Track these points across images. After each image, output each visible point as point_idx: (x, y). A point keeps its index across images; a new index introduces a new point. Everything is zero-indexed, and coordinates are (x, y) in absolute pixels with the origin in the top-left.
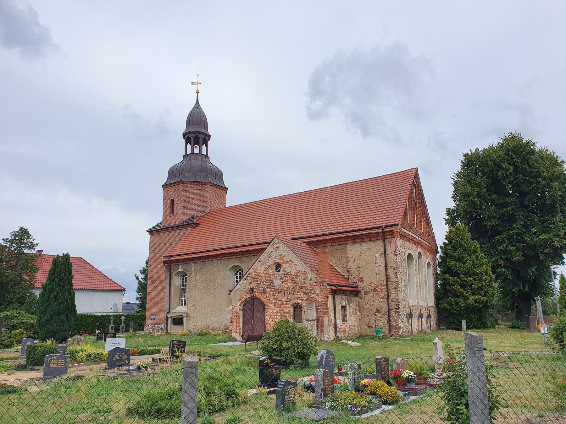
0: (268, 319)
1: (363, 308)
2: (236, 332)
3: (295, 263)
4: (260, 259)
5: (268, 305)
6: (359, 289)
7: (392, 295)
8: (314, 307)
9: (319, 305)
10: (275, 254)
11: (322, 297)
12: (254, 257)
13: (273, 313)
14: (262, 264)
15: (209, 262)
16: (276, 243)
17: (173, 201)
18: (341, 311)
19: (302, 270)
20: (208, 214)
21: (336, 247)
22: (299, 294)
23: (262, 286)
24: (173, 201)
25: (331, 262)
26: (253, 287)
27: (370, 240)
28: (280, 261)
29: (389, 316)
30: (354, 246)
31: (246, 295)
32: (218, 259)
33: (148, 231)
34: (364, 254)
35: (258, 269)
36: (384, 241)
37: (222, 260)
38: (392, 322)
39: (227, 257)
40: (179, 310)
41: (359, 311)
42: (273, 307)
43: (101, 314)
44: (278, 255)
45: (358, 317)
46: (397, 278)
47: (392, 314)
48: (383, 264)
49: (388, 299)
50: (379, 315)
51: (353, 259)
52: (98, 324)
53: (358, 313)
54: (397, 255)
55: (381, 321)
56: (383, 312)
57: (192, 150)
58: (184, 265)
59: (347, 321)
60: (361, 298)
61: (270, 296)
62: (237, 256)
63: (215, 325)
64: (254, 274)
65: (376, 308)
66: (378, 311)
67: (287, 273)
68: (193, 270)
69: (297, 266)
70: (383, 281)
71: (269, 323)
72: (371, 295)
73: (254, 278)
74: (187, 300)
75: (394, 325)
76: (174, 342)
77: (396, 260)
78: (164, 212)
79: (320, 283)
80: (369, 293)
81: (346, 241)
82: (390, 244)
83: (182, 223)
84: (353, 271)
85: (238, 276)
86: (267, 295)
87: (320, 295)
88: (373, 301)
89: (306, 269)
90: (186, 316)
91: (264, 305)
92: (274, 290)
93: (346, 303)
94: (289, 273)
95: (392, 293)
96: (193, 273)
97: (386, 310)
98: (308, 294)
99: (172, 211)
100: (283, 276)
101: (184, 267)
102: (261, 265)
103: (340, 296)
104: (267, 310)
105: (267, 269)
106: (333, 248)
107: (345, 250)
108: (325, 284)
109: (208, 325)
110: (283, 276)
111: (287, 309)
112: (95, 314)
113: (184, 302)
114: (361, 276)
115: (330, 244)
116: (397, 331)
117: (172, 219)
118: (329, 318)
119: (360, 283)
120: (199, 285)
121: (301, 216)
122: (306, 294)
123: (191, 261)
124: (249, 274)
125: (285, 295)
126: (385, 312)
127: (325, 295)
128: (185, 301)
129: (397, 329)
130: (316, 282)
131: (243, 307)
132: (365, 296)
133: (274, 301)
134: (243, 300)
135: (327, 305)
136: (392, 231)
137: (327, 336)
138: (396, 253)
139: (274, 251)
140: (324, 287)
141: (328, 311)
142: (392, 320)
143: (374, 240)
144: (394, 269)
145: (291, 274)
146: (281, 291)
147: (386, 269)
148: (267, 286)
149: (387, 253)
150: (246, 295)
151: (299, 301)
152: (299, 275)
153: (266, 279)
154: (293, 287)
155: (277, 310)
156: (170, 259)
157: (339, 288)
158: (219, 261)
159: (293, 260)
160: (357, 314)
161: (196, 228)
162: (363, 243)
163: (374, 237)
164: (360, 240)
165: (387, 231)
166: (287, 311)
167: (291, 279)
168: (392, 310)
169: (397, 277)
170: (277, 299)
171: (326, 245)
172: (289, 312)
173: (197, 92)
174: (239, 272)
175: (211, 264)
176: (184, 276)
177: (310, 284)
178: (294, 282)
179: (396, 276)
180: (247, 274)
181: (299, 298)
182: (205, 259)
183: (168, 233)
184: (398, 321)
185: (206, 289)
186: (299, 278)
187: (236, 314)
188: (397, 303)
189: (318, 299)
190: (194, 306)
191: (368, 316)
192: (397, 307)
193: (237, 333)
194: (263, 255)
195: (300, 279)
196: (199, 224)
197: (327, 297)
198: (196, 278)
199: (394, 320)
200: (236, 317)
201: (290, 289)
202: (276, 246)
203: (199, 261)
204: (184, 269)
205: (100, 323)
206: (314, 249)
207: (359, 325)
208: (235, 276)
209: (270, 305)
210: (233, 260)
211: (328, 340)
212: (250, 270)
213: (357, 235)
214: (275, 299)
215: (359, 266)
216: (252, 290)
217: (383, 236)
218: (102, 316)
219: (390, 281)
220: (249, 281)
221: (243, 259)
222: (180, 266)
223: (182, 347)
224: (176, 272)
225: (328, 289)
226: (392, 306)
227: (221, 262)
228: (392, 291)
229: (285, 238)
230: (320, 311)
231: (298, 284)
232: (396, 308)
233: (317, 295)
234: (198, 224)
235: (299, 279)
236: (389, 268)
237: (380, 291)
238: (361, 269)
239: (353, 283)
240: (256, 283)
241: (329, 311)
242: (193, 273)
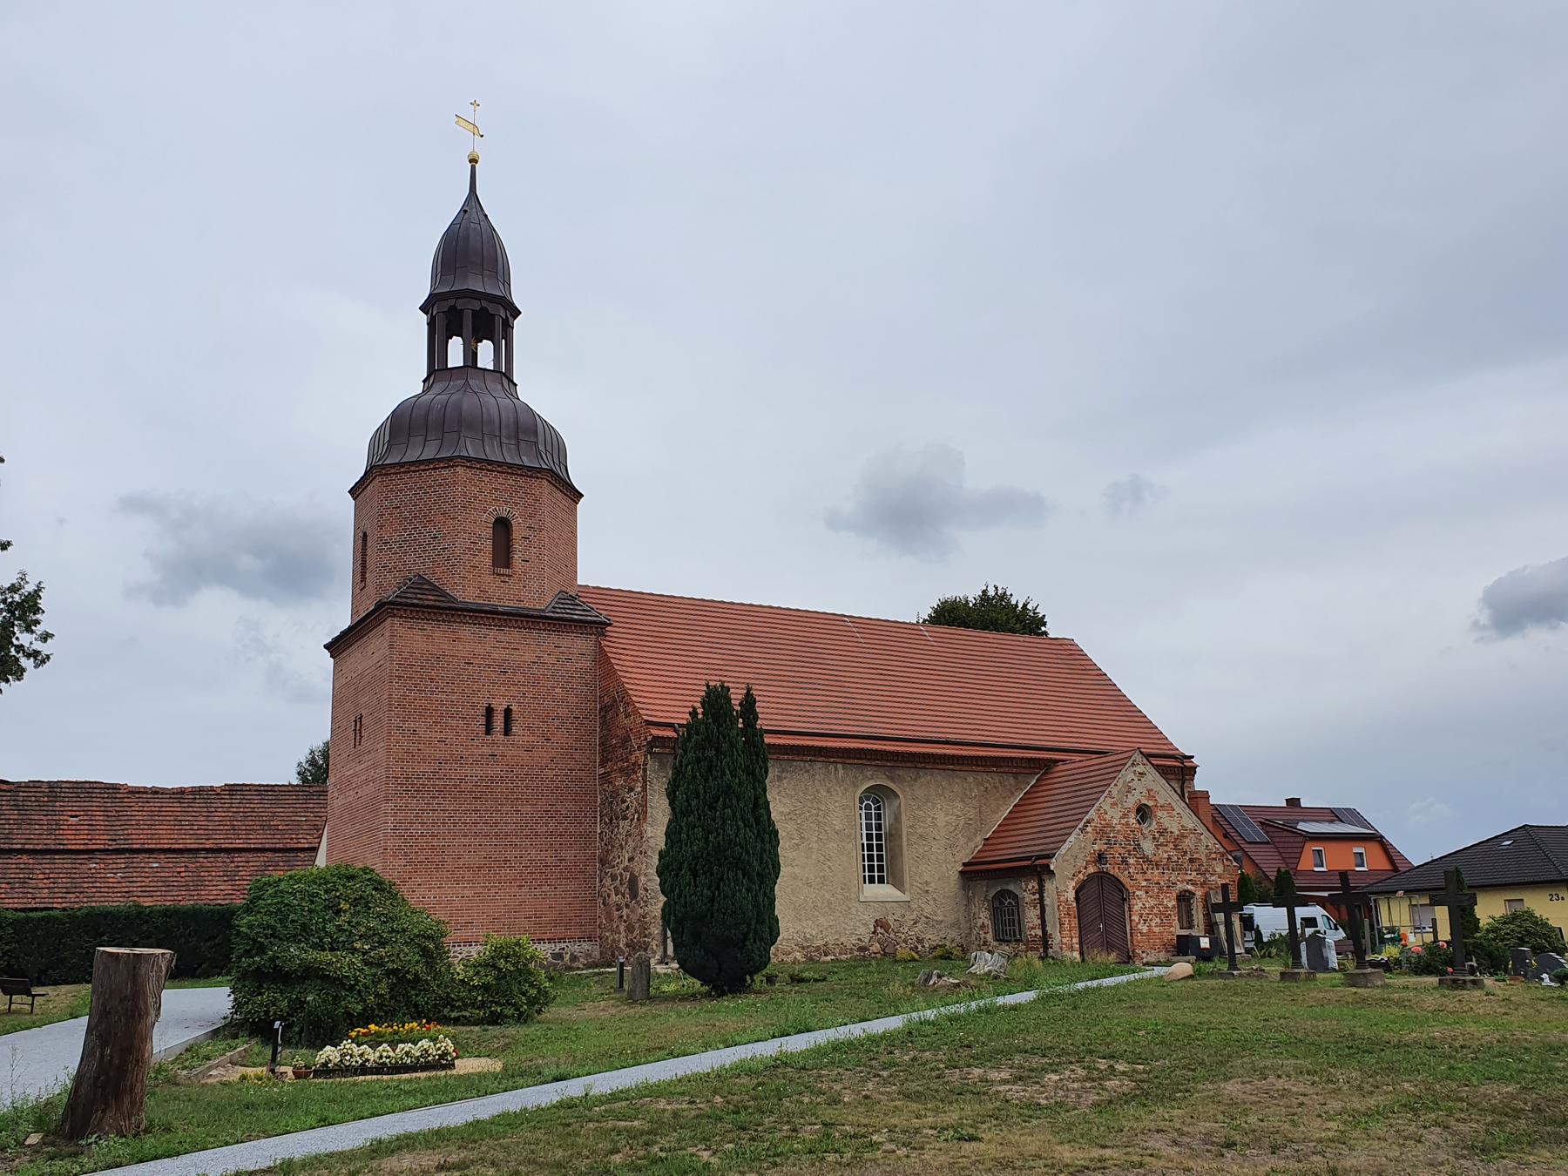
0: (1137, 921)
5: (1134, 893)
12: (927, 771)
13: (1146, 908)
15: (802, 763)
19: (1191, 826)
22: (1189, 872)
31: (1086, 868)
44: (1145, 791)
57: (471, 355)
58: (882, 769)
61: (1137, 873)
62: (884, 763)
63: (831, 939)
73: (1102, 833)
79: (1222, 855)
86: (1131, 870)
92: (1144, 862)
100: (1157, 836)
102: (1114, 805)
109: (807, 940)
121: (691, 659)
122: (1202, 874)
124: (1088, 822)
125: (1164, 873)
133: (1144, 883)
139: (1136, 779)
140: (1229, 863)
145: (1171, 832)
146: (1156, 865)
148: (1129, 851)
150: (1086, 868)
151: (1190, 887)
153: (1125, 837)
155: (1152, 902)
158: (832, 768)
159: (1174, 805)
170: (1150, 880)
173: (470, 162)
183: (484, 630)
185: (796, 836)
186: (1187, 841)
187: (1068, 908)
194: (1116, 785)
195: (1188, 843)
200: (1069, 914)
209: (1138, 893)
214: (1146, 880)
216: (1101, 858)
220: (1091, 836)
221: (897, 772)
227: (836, 769)
240: (1106, 844)
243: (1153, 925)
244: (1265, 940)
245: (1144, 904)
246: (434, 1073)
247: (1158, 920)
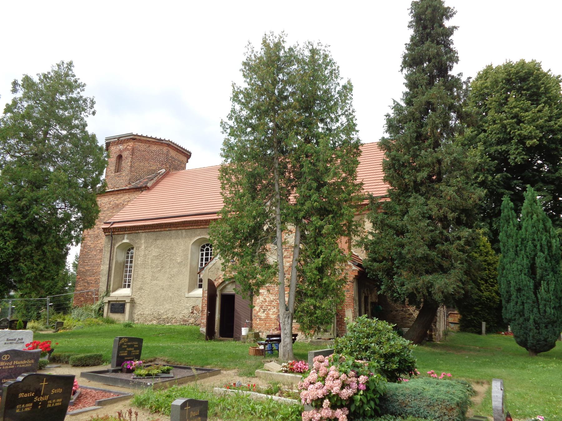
0: (257, 310)
13: (266, 301)
15: (166, 232)
32: (179, 228)
37: (184, 231)
39: (191, 226)
40: (123, 293)
42: (265, 293)
55: (410, 319)
63: (170, 315)
71: (258, 316)
74: (132, 281)
76: (122, 341)
85: (204, 253)
109: (159, 315)
113: (127, 283)
120: (150, 261)
128: (128, 282)
158: (180, 232)
174: (206, 247)
176: (129, 250)
182: (161, 228)
190: (141, 289)
203: (153, 230)
208: (200, 253)
210: (199, 231)
223: (136, 349)
224: (120, 243)
225: (354, 270)
227: (182, 233)
243: (271, 313)
244: (377, 301)
245: (265, 299)
246: (154, 345)
247: (275, 310)
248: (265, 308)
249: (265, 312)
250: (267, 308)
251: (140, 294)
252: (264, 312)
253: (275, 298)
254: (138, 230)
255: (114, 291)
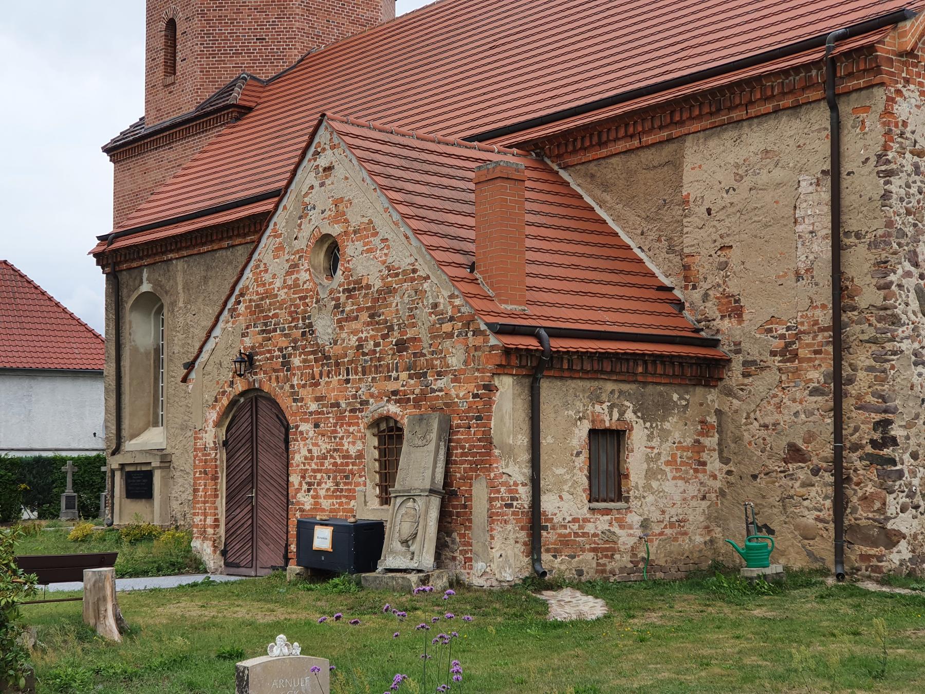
1: (738, 440)
2: (203, 534)
3: (383, 233)
4: (275, 224)
6: (725, 349)
7: (861, 374)
8: (434, 435)
9: (459, 426)
10: (321, 199)
11: (471, 387)
14: (280, 248)
15: (224, 253)
16: (324, 149)
17: (171, 25)
18: (585, 455)
20: (295, 67)
21: (647, 156)
22: (394, 374)
23: (279, 345)
24: (171, 25)
25: (623, 228)
26: (253, 348)
27: (776, 111)
28: (335, 230)
29: (841, 481)
30: (713, 143)
31: (232, 384)
33: (107, 150)
34: (748, 182)
35: (266, 271)
36: (834, 108)
38: (855, 510)
41: (721, 452)
42: (311, 434)
43: (37, 454)
44: (329, 203)
45: (711, 483)
46: (882, 292)
47: (856, 470)
48: (824, 225)
49: (839, 396)
50: (802, 475)
51: (703, 209)
52: (23, 486)
53: (714, 464)
54: (890, 173)
55: (806, 503)
56: (815, 460)
59: (627, 500)
60: (729, 393)
61: (304, 386)
64: (257, 294)
65: (789, 439)
66: (795, 454)
67: (356, 282)
68: (180, 287)
69: (388, 247)
70: (824, 306)
72: (771, 377)
75: (863, 522)
77: (886, 195)
78: (150, 71)
79: (468, 322)
80: (762, 369)
81: (681, 123)
82: (863, 122)
83: (197, 110)
84: (703, 266)
86: (295, 383)
87: (467, 381)
88: (778, 406)
89: (420, 260)
90: (158, 464)
91: (287, 428)
92: (316, 360)
93: (629, 415)
94: (364, 284)
95: (860, 364)
96: (181, 300)
97: (828, 452)
98: (425, 375)
99: (171, 67)
101: (157, 276)
103: (587, 384)
104: (293, 446)
105: (294, 267)
106: (633, 161)
107: (676, 165)
108: (483, 327)
110: (343, 297)
111: (354, 443)
112: (11, 455)
114: (733, 288)
115: (621, 146)
116: (873, 551)
117: (171, 97)
118: (493, 488)
119: (727, 321)
123: (171, 251)
126: (825, 460)
127: (483, 379)
129: (875, 544)
130: (452, 319)
131: (227, 432)
132: (746, 381)
133: (313, 407)
134: (225, 401)
135: (485, 426)
136: (871, 48)
137: (479, 566)
138: (888, 162)
140: (479, 341)
141: (489, 454)
142: (855, 500)
143: (796, 107)
144: (873, 245)
145: (368, 287)
147: (837, 248)
148: (295, 341)
149: (846, 166)
151: (393, 409)
152: (395, 290)
153: (290, 313)
154: (377, 345)
156: (116, 245)
157: (558, 344)
159: (378, 222)
160: (709, 467)
161: (239, 123)
162: (750, 126)
163: (791, 92)
164: (735, 115)
165: (848, 54)
166: (353, 451)
167: (368, 308)
168: (855, 447)
169: (888, 286)
171: (604, 152)
172: (360, 455)
175: (230, 263)
177: (432, 329)
178: (377, 323)
179: (882, 282)
180: (237, 292)
181: (395, 393)
184: (877, 505)
186: (395, 300)
188: (878, 417)
189: (457, 396)
191: (755, 477)
192: (877, 436)
193: (205, 539)
196: (250, 109)
197: (490, 388)
198: (189, 316)
199: (864, 498)
201: (364, 354)
202: (323, 162)
204: (157, 284)
205: (30, 484)
206: (564, 174)
207: (714, 518)
211: (486, 585)
212: (244, 277)
213: (721, 89)
215: (727, 241)
217: (832, 81)
218: (38, 460)
219: (854, 309)
222: (145, 275)
224: (135, 296)
225: (493, 347)
226: (856, 429)
228: (862, 358)
229: (421, 132)
230: (462, 454)
231: (391, 328)
232: (873, 443)
233: (456, 380)
234: (244, 107)
235: (393, 309)
236: (853, 240)
237: (810, 360)
238: (734, 256)
239: (699, 321)
240: (263, 331)
241: (496, 452)
242: (181, 300)
243: (322, 493)
248: (310, 477)
249: (312, 492)
250: (315, 478)
251: (184, 443)
252: (309, 490)
253: (329, 447)
254: (163, 253)
255: (133, 436)
